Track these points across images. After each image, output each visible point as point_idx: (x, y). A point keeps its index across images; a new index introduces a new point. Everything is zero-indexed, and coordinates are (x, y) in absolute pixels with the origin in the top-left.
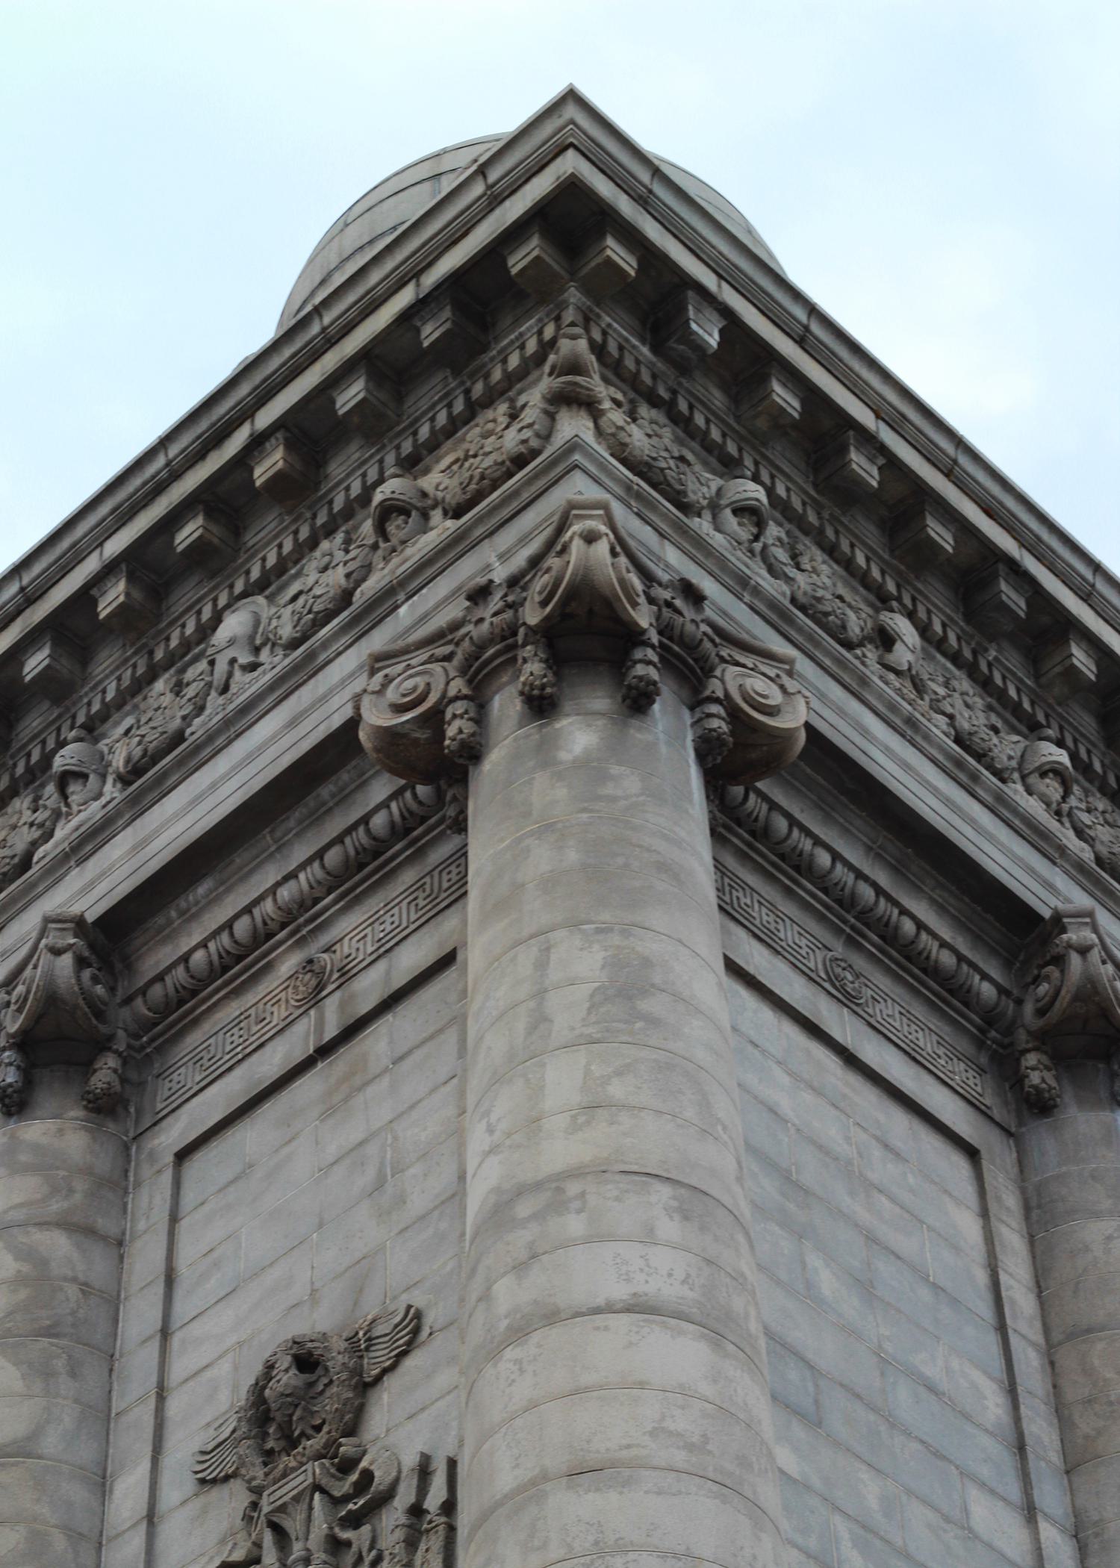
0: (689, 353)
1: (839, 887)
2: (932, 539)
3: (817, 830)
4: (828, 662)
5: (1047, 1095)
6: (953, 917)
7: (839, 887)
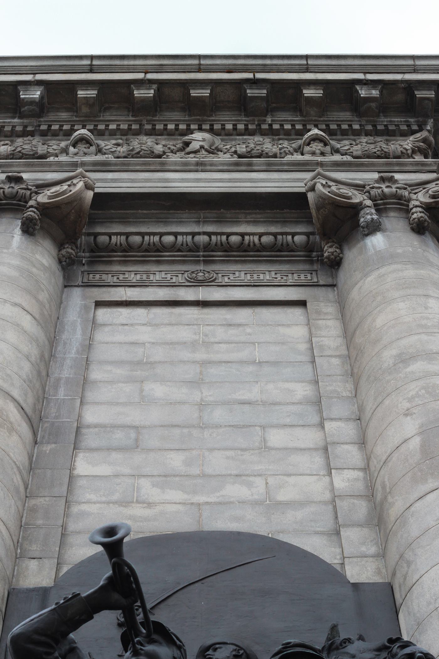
0: (32, 107)
1: (185, 245)
2: (195, 96)
3: (158, 231)
4: (138, 168)
5: (332, 257)
6: (265, 222)
7: (185, 245)
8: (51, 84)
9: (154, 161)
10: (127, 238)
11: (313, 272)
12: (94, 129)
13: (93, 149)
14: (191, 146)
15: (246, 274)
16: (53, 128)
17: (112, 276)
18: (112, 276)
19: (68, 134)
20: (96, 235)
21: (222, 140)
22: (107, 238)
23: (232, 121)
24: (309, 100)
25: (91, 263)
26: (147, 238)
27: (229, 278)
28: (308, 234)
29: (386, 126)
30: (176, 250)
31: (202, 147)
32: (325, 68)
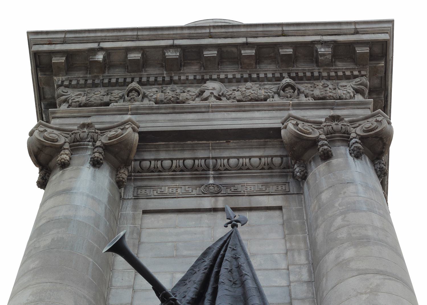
8: (119, 50)
17: (137, 189)
24: (209, 59)
26: (241, 160)
28: (282, 157)
30: (172, 171)
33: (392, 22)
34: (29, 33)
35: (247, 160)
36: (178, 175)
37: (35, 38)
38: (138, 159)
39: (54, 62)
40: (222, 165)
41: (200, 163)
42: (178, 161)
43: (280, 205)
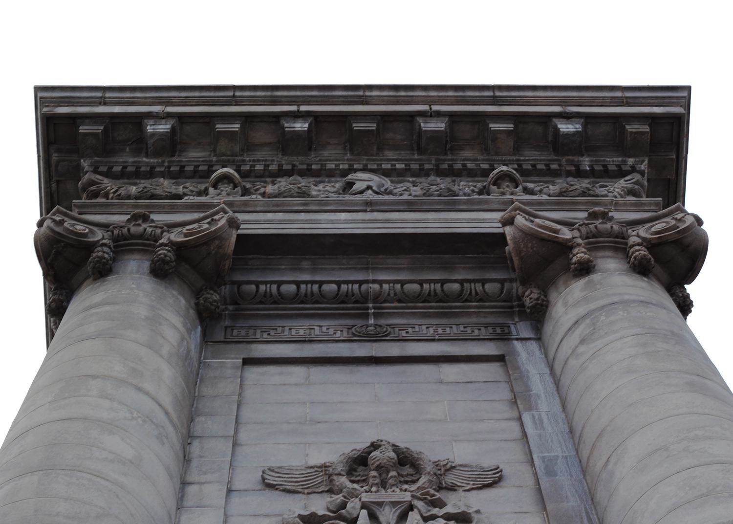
9: (308, 204)
10: (320, 287)
11: (454, 326)
12: (264, 170)
13: (238, 189)
14: (355, 187)
15: (427, 328)
16: (172, 169)
18: (427, 328)
19: (485, 173)
20: (240, 284)
21: (392, 182)
22: (253, 287)
23: (544, 160)
25: (234, 317)
27: (269, 334)
29: (619, 166)
31: (369, 187)
32: (356, 99)
33: (688, 89)
34: (38, 89)
35: (438, 286)
36: (456, 307)
37: (45, 96)
38: (325, 281)
39: (426, 130)
40: (473, 292)
41: (268, 290)
42: (309, 286)
43: (503, 353)
